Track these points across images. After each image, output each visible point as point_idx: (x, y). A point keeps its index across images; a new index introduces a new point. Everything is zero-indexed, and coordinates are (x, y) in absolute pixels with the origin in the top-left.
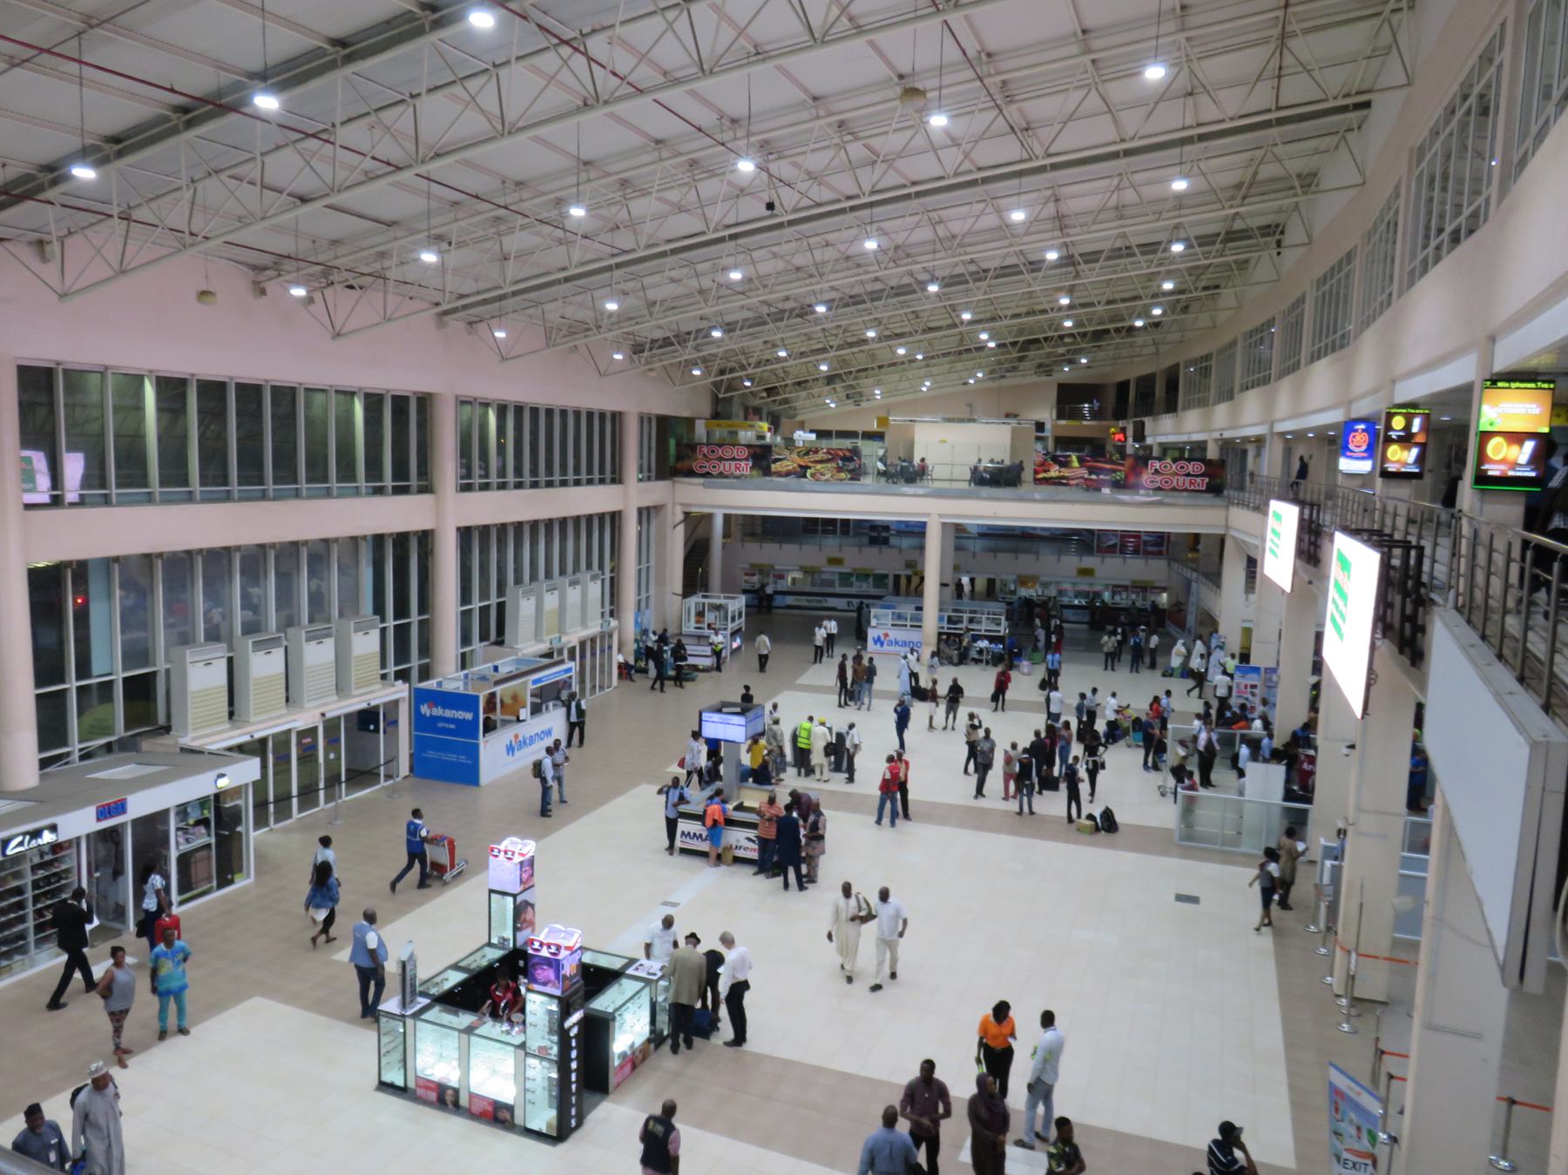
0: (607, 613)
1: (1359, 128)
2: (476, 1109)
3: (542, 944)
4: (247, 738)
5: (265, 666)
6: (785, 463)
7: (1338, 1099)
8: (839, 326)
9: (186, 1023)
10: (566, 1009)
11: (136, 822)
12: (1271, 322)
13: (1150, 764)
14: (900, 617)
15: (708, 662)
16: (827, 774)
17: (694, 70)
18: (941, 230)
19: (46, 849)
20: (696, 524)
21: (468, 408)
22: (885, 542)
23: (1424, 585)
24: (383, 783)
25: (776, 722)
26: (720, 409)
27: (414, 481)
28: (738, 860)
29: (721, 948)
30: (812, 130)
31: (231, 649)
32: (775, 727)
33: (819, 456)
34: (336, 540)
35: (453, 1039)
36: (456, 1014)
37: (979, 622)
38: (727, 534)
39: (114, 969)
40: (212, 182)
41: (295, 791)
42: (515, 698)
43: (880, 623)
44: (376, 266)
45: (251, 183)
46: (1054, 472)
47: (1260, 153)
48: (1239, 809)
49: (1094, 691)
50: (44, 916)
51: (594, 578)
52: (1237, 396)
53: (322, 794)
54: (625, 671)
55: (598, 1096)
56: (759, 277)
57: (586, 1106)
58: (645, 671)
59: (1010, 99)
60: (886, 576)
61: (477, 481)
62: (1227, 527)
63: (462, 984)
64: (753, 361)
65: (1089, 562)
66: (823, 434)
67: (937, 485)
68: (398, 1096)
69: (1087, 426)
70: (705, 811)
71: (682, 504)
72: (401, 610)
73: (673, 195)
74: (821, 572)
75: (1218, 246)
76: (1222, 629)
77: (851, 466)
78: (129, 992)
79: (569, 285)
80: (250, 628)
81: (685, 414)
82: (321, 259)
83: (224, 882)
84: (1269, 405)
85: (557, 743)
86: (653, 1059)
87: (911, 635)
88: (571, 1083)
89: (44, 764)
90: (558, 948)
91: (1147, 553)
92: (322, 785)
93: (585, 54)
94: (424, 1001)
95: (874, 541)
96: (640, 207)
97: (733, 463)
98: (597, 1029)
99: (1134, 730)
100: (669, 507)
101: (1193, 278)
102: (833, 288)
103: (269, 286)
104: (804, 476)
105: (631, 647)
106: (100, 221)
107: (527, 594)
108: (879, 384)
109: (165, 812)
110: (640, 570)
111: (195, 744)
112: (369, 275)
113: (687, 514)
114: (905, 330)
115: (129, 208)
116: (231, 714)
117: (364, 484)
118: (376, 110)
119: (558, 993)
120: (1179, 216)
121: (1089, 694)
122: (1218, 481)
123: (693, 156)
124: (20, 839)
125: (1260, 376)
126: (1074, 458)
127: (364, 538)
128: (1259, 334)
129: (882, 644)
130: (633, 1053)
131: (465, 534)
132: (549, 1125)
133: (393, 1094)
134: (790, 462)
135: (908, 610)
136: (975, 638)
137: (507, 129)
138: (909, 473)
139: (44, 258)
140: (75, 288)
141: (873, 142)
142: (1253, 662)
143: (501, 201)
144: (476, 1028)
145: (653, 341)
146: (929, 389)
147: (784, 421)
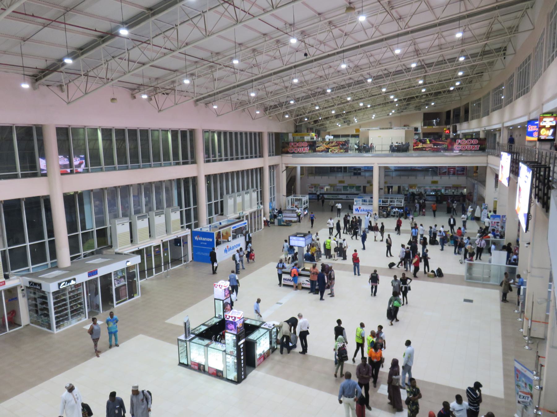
0: (259, 204)
1: (532, 7)
2: (211, 372)
3: (229, 317)
4: (137, 249)
5: (142, 225)
6: (321, 147)
7: (517, 372)
8: (338, 97)
9: (118, 343)
10: (239, 338)
11: (101, 277)
12: (502, 85)
13: (457, 252)
14: (365, 201)
15: (295, 219)
16: (336, 258)
17: (271, 8)
18: (372, 59)
19: (73, 286)
20: (290, 171)
21: (207, 134)
22: (360, 174)
23: (551, 181)
24: (183, 263)
25: (318, 240)
26: (297, 129)
27: (190, 160)
28: (303, 288)
29: (297, 318)
30: (318, 26)
31: (130, 219)
32: (317, 241)
33: (333, 144)
34: (164, 181)
35: (202, 349)
36: (203, 340)
37: (394, 202)
38: (302, 174)
39: (93, 325)
40: (113, 61)
41: (154, 267)
42: (227, 233)
43: (358, 204)
44: (172, 86)
45: (125, 60)
46: (420, 146)
47: (492, 20)
48: (489, 267)
49: (436, 226)
50: (73, 308)
51: (254, 191)
52: (490, 114)
53: (163, 267)
54: (266, 223)
55: (252, 368)
56: (305, 81)
57: (247, 371)
58: (273, 223)
59: (392, 8)
60: (360, 187)
61: (212, 159)
62: (487, 163)
63: (206, 330)
64: (307, 111)
65: (436, 178)
66: (335, 136)
67: (377, 153)
68: (186, 367)
69: (435, 128)
70: (291, 271)
71: (285, 164)
72: (188, 204)
73: (271, 53)
74: (336, 186)
75: (478, 58)
76: (487, 201)
77: (345, 147)
78: (99, 332)
79: (239, 88)
80: (137, 212)
81: (285, 131)
82: (152, 85)
83: (131, 297)
84: (502, 116)
85: (241, 249)
86: (271, 356)
87: (369, 208)
88: (242, 364)
89: (72, 259)
90: (235, 318)
91: (458, 174)
92: (163, 264)
93: (233, 5)
94: (193, 336)
95: (355, 174)
96: (260, 59)
97: (302, 148)
98: (250, 346)
99: (451, 239)
100: (280, 165)
101: (472, 70)
102: (334, 83)
103: (137, 95)
104: (328, 152)
105: (268, 215)
106: (79, 77)
107: (230, 197)
108: (356, 116)
109: (111, 273)
110: (271, 188)
111: (120, 251)
112: (169, 89)
113: (287, 167)
114: (362, 97)
115: (88, 72)
116: (132, 241)
117: (130, 165)
118: (164, 32)
119: (235, 333)
120: (442, 52)
121: (433, 227)
122: (484, 146)
123: (277, 38)
124: (64, 283)
125: (499, 106)
126: (428, 140)
127: (174, 180)
128: (498, 91)
129: (358, 211)
130: (264, 354)
131: (208, 177)
132: (235, 378)
133: (184, 367)
134: (323, 147)
135: (368, 199)
136: (393, 208)
137: (208, 34)
138: (365, 148)
139: (62, 91)
140: (72, 100)
141: (342, 28)
142: (497, 214)
143: (211, 60)
144: (210, 345)
145: (271, 106)
146: (372, 116)
147: (322, 132)
